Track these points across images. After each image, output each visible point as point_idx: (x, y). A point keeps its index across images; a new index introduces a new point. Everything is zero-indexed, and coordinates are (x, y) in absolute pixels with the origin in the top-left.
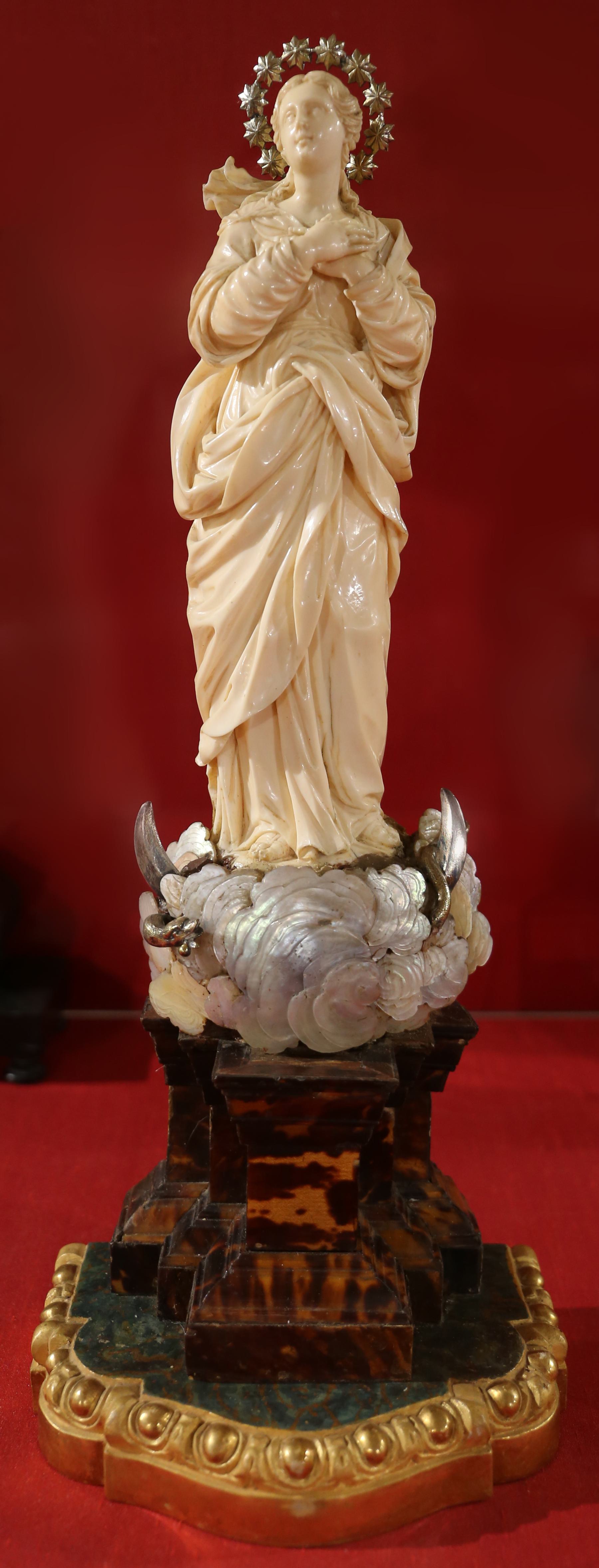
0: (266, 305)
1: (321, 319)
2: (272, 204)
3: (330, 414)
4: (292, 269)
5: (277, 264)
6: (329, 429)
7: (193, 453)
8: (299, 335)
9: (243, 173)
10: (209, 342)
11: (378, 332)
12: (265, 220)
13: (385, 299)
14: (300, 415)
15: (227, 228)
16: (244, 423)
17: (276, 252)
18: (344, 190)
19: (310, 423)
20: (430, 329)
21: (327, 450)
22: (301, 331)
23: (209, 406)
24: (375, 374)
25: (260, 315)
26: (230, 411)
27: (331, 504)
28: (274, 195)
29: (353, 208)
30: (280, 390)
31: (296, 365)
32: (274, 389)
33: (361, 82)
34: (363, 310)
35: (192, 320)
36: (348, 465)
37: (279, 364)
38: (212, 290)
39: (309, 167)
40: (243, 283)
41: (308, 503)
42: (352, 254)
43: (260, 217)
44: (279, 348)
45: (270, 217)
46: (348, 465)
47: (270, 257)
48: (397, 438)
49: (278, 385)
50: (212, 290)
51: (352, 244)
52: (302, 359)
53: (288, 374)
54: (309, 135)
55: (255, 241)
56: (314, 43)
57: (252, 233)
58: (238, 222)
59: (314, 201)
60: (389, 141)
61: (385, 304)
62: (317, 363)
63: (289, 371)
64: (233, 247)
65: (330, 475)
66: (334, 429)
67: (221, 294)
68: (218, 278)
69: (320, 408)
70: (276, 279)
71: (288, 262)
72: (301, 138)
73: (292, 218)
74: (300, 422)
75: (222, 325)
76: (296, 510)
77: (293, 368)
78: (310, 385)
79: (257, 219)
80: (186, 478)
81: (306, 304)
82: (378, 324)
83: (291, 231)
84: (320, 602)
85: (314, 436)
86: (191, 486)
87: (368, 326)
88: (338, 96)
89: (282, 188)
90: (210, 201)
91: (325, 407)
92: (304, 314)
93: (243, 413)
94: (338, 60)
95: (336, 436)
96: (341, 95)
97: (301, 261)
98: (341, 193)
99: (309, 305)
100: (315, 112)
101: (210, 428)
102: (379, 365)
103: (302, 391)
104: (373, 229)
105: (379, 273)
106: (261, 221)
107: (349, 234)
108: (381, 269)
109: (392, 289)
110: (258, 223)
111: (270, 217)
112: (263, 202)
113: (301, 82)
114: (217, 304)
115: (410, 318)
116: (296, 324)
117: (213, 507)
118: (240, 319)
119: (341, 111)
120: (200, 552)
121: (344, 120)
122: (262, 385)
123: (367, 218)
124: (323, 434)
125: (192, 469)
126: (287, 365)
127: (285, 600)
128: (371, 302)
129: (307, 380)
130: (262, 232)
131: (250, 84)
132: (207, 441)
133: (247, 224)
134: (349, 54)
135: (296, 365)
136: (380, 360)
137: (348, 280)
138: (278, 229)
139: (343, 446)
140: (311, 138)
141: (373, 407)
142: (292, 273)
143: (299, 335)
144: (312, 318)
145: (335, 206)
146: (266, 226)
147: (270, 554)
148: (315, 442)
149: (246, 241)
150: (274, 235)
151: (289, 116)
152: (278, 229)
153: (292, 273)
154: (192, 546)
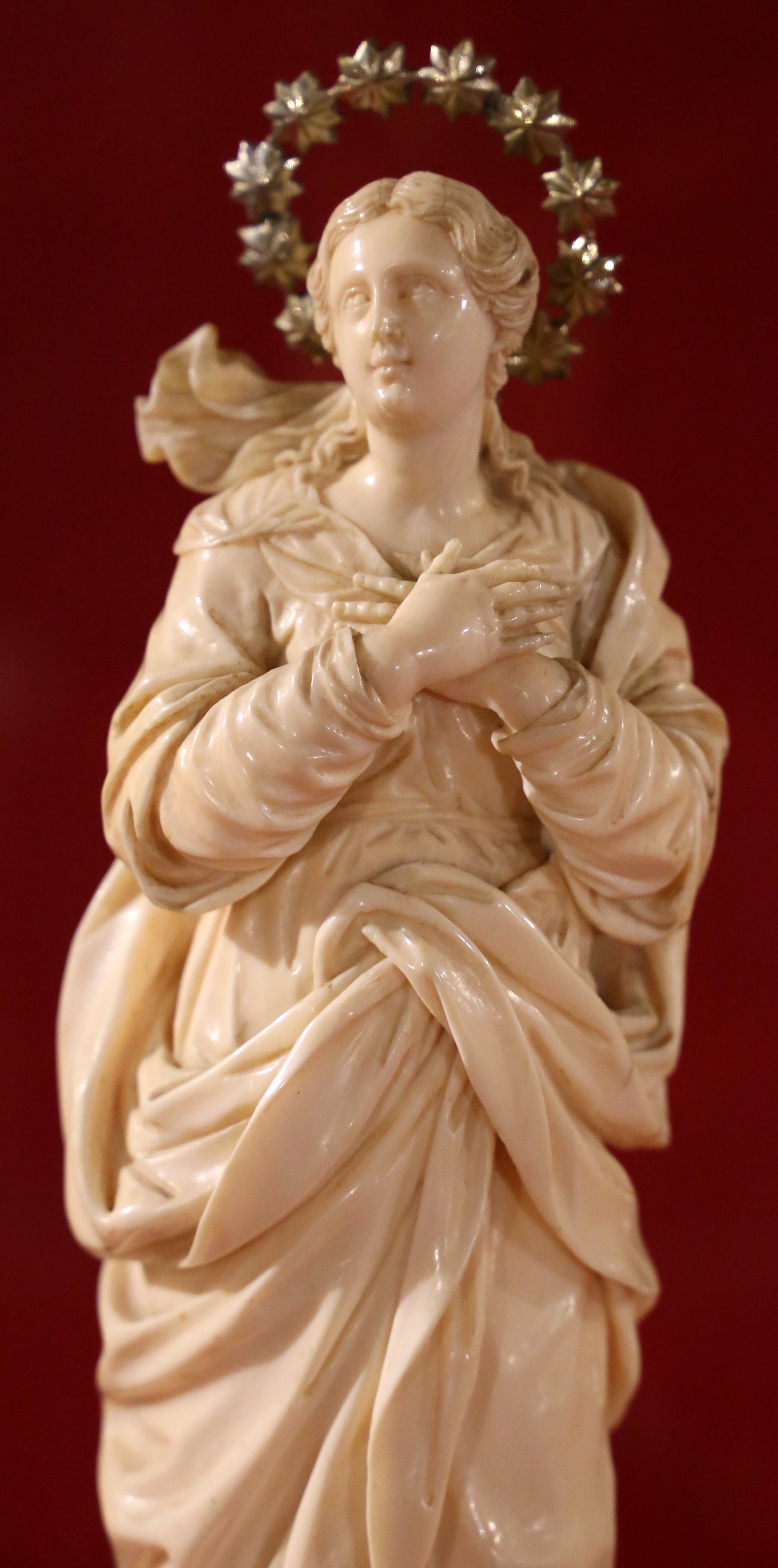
0: (296, 797)
1: (432, 821)
2: (312, 493)
3: (454, 1050)
4: (360, 715)
5: (325, 703)
6: (454, 1086)
7: (117, 1098)
8: (383, 837)
9: (241, 374)
10: (157, 855)
11: (574, 837)
12: (294, 546)
13: (593, 766)
14: (383, 1060)
15: (200, 543)
16: (245, 1066)
17: (318, 670)
18: (494, 451)
19: (408, 1072)
20: (710, 795)
21: (450, 1137)
22: (384, 827)
23: (155, 962)
24: (572, 916)
25: (281, 821)
26: (205, 1023)
27: (460, 1274)
28: (316, 462)
29: (517, 493)
30: (333, 994)
31: (371, 932)
32: (317, 992)
33: (537, 158)
34: (541, 787)
35: (114, 795)
36: (502, 1159)
37: (331, 923)
38: (165, 738)
39: (403, 424)
40: (238, 744)
41: (404, 1263)
42: (511, 656)
43: (282, 535)
44: (330, 872)
45: (308, 534)
46: (502, 1159)
47: (305, 686)
48: (627, 1081)
49: (330, 976)
50: (165, 738)
51: (511, 635)
52: (389, 920)
53: (349, 953)
54: (404, 354)
55: (269, 596)
56: (417, 58)
57: (263, 575)
58: (225, 544)
59: (416, 489)
60: (609, 295)
61: (592, 771)
62: (425, 931)
63: (355, 944)
64: (218, 618)
65: (457, 1188)
66: (467, 1085)
67: (184, 753)
68: (176, 715)
69: (433, 1033)
70: (323, 739)
71: (352, 701)
72: (385, 363)
73: (363, 544)
74: (384, 1075)
75: (185, 828)
76: (374, 1279)
77: (364, 938)
78: (406, 983)
79: (273, 540)
80: (97, 1180)
81: (397, 762)
82: (576, 822)
83: (361, 585)
84: (435, 1514)
85: (419, 1100)
86: (110, 1205)
87: (551, 821)
88: (475, 252)
89: (337, 439)
90: (157, 437)
91: (442, 1031)
92: (393, 787)
93: (240, 1037)
94: (478, 103)
95: (473, 1105)
96: (482, 248)
97: (380, 694)
98: (485, 453)
99: (406, 767)
100: (418, 295)
101: (158, 1033)
102: (584, 900)
103: (388, 997)
104: (566, 539)
105: (579, 705)
106: (285, 547)
107: (502, 610)
108: (584, 692)
109: (613, 739)
110: (279, 551)
111: (308, 534)
112: (290, 483)
113: (381, 209)
114: (175, 783)
115: (659, 781)
116: (372, 809)
117: (163, 1246)
118: (229, 827)
119: (481, 283)
120: (136, 1349)
121: (492, 304)
122: (290, 963)
123: (552, 511)
124: (440, 1093)
125: (113, 1155)
126: (350, 931)
127: (345, 1502)
128: (556, 773)
129: (396, 969)
130: (287, 576)
131: (254, 144)
132: (151, 1073)
133: (250, 551)
134: (508, 88)
135: (371, 932)
136: (583, 885)
137: (501, 715)
138: (328, 572)
139: (488, 1122)
140: (408, 363)
141: (567, 1014)
142: (360, 725)
143: (383, 837)
144: (411, 794)
145: (473, 499)
146: (296, 560)
147: (309, 1389)
148: (422, 1115)
149: (247, 597)
150: (318, 588)
151: (352, 295)
152: (328, 572)
153: (360, 725)
154: (114, 1329)
